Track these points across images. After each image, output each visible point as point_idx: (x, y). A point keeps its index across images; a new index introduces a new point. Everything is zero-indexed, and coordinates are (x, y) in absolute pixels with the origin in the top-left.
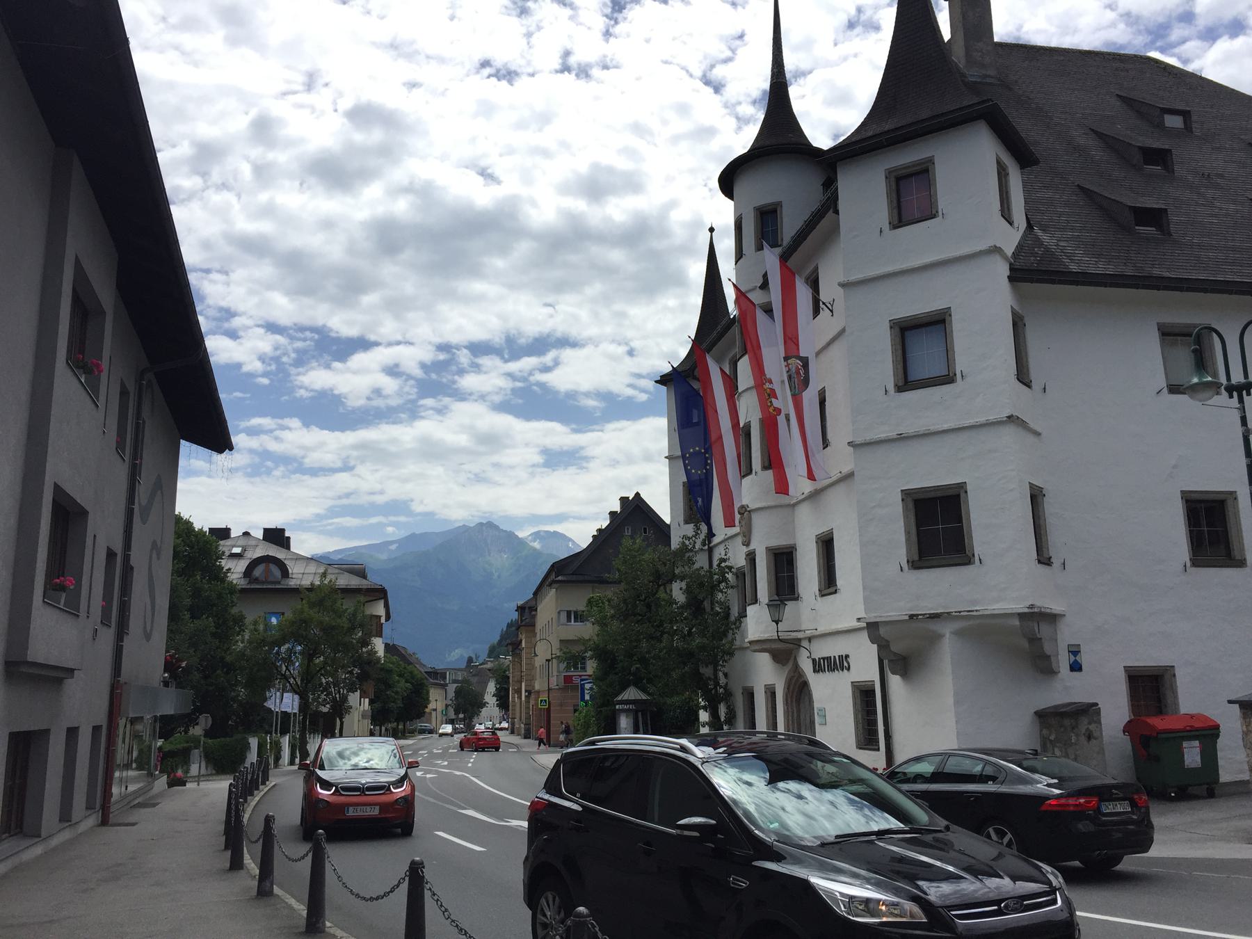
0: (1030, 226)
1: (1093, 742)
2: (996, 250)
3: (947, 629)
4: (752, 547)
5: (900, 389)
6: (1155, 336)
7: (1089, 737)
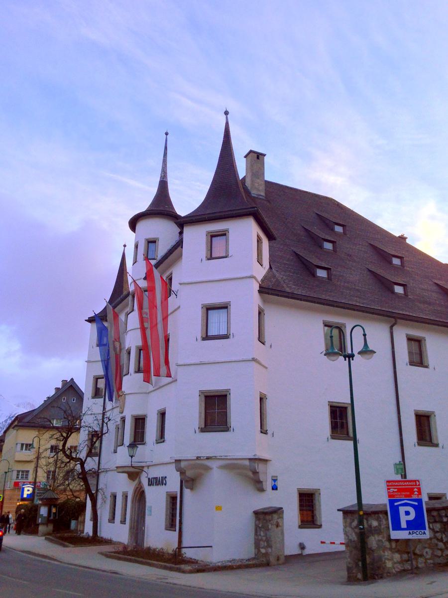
0: (271, 268)
1: (279, 528)
2: (252, 277)
3: (214, 464)
4: (123, 415)
5: (204, 339)
6: (322, 325)
7: (277, 526)
